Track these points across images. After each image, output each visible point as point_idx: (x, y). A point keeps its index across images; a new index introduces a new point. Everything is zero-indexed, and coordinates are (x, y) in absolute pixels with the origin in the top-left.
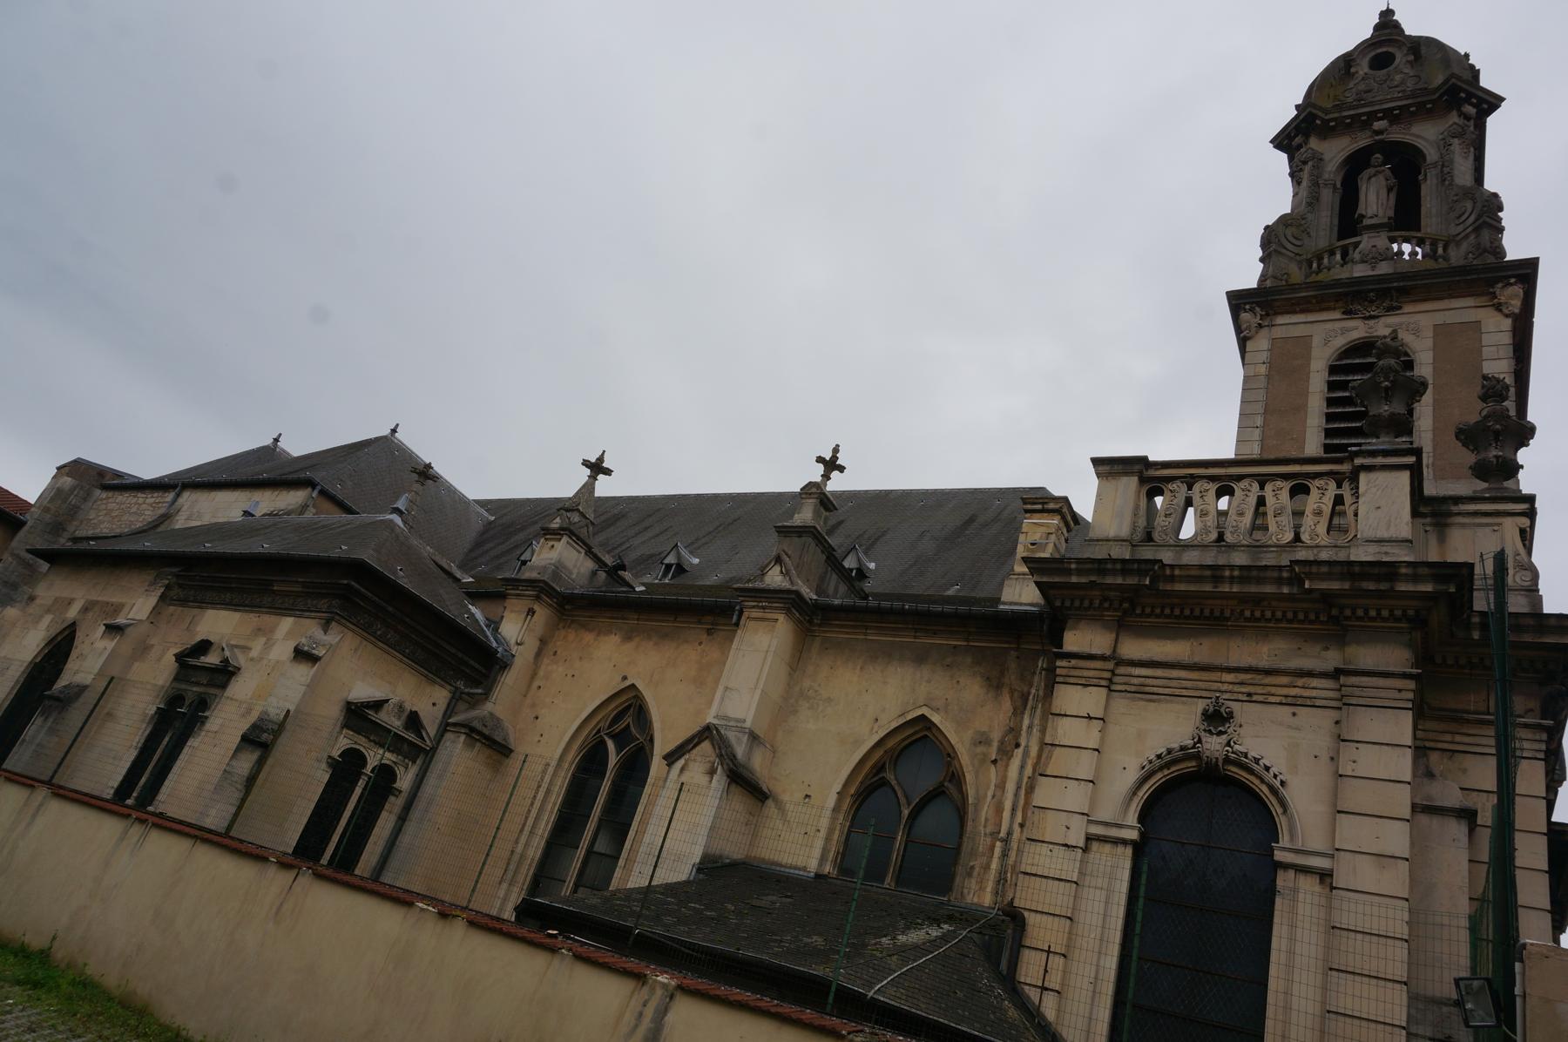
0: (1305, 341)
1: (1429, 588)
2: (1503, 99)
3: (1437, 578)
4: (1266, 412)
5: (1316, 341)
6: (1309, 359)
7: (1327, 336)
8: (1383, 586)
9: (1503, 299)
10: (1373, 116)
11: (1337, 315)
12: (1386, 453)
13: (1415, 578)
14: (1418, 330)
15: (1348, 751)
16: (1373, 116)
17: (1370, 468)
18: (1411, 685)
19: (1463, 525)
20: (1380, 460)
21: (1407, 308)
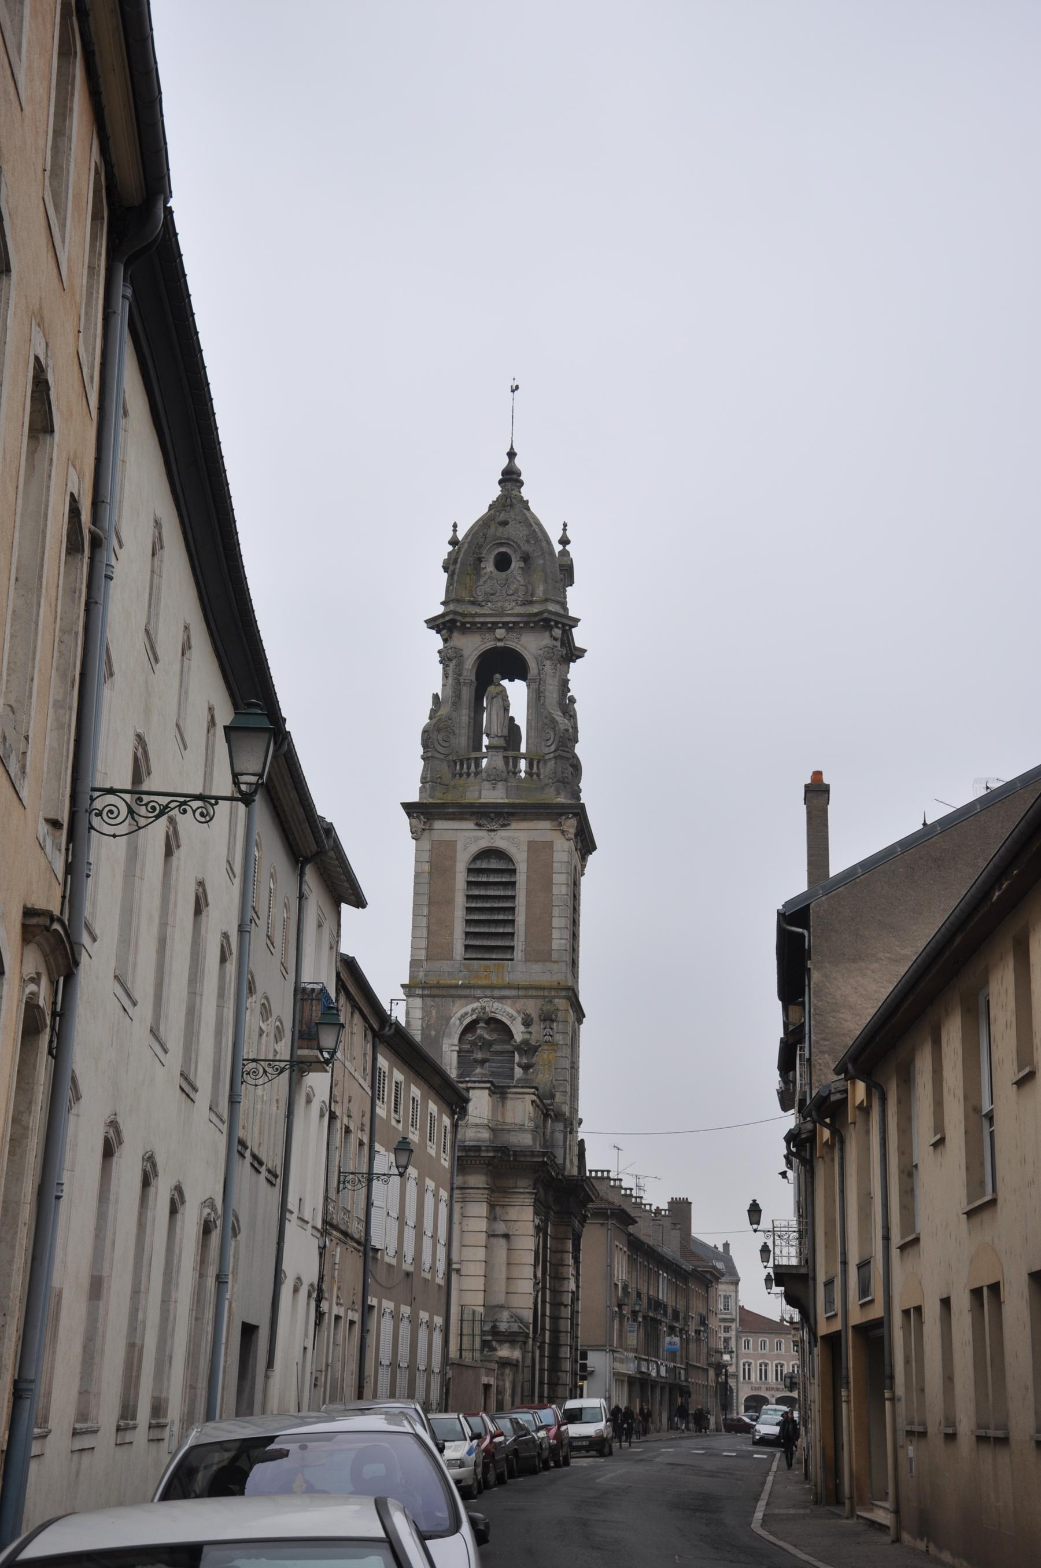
0: (452, 845)
1: (491, 1154)
2: (585, 651)
3: (495, 1151)
4: (430, 903)
5: (460, 846)
6: (455, 861)
7: (468, 839)
8: (477, 1154)
9: (565, 829)
10: (495, 625)
11: (470, 825)
12: (479, 1082)
13: (487, 1151)
14: (515, 839)
15: (465, 1221)
16: (495, 625)
17: (474, 1088)
18: (486, 1192)
19: (512, 1099)
20: (477, 1085)
21: (514, 825)
